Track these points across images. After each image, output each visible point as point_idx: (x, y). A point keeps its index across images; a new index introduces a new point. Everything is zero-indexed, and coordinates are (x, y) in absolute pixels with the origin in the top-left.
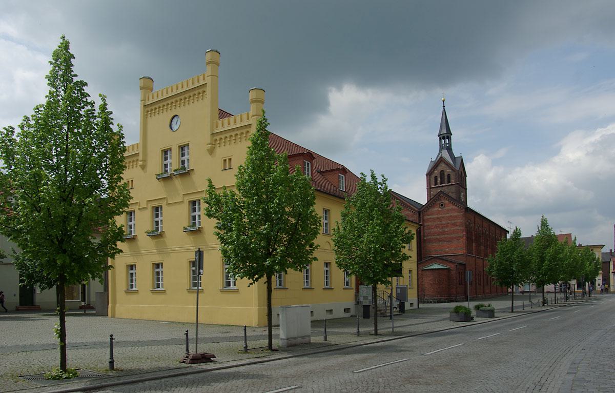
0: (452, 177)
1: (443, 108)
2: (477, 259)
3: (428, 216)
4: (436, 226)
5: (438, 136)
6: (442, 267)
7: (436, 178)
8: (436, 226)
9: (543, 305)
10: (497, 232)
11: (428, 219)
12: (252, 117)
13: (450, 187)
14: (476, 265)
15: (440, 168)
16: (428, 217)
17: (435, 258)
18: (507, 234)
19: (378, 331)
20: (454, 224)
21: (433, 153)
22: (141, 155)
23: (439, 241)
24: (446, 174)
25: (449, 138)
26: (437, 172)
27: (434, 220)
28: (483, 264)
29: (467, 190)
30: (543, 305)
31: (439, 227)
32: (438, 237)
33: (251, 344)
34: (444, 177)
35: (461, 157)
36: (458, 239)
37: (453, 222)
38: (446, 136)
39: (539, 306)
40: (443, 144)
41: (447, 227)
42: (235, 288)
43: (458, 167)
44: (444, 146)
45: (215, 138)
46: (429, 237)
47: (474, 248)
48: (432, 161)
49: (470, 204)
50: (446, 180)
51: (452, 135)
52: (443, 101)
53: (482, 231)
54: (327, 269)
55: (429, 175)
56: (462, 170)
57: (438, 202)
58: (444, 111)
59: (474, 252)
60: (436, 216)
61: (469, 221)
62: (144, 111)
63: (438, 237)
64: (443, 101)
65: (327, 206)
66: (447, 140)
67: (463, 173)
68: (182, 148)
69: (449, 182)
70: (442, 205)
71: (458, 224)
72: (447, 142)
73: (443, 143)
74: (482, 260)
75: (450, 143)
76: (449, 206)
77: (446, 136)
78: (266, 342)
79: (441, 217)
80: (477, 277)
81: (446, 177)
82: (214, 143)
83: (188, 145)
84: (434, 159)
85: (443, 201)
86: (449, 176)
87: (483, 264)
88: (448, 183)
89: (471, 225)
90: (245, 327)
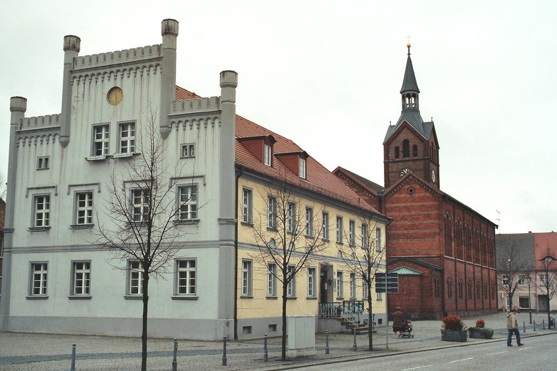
0: (420, 149)
1: (407, 56)
2: (458, 264)
3: (392, 203)
4: (403, 218)
5: (401, 93)
6: (411, 273)
7: (397, 149)
8: (403, 218)
9: (550, 328)
10: (482, 226)
11: (392, 207)
12: (222, 102)
13: (418, 162)
14: (456, 271)
15: (402, 137)
16: (393, 205)
17: (400, 259)
18: (496, 229)
19: (373, 347)
20: (428, 217)
21: (393, 114)
22: (63, 129)
23: (407, 237)
24: (411, 145)
25: (416, 96)
26: (399, 142)
27: (400, 209)
28: (465, 269)
29: (440, 167)
30: (550, 328)
31: (407, 220)
32: (406, 232)
33: (270, 354)
34: (409, 148)
35: (432, 123)
36: (432, 235)
37: (426, 213)
38: (410, 89)
39: (544, 329)
40: (407, 105)
41: (417, 219)
42: (192, 295)
43: (427, 137)
44: (408, 106)
45: (74, 75)
46: (394, 232)
47: (453, 247)
48: (391, 127)
49: (445, 187)
50: (411, 152)
51: (419, 92)
52: (409, 47)
53: (469, 228)
54: (311, 276)
55: (387, 145)
56: (433, 140)
57: (407, 187)
58: (409, 62)
59: (453, 253)
60: (403, 204)
61: (447, 213)
62: (70, 78)
63: (406, 232)
64: (409, 47)
65: (291, 199)
66: (413, 99)
67: (434, 142)
68: (123, 126)
69: (415, 155)
70: (411, 191)
71: (432, 216)
72: (413, 102)
73: (407, 102)
74: (463, 265)
75: (417, 103)
76: (422, 193)
77: (410, 89)
78: (280, 354)
79: (410, 206)
80: (458, 286)
81: (411, 149)
82: (170, 126)
83: (133, 124)
84: (394, 123)
85: (412, 186)
86: (415, 147)
87: (465, 269)
88: (414, 156)
89: (450, 218)
90: (265, 339)
